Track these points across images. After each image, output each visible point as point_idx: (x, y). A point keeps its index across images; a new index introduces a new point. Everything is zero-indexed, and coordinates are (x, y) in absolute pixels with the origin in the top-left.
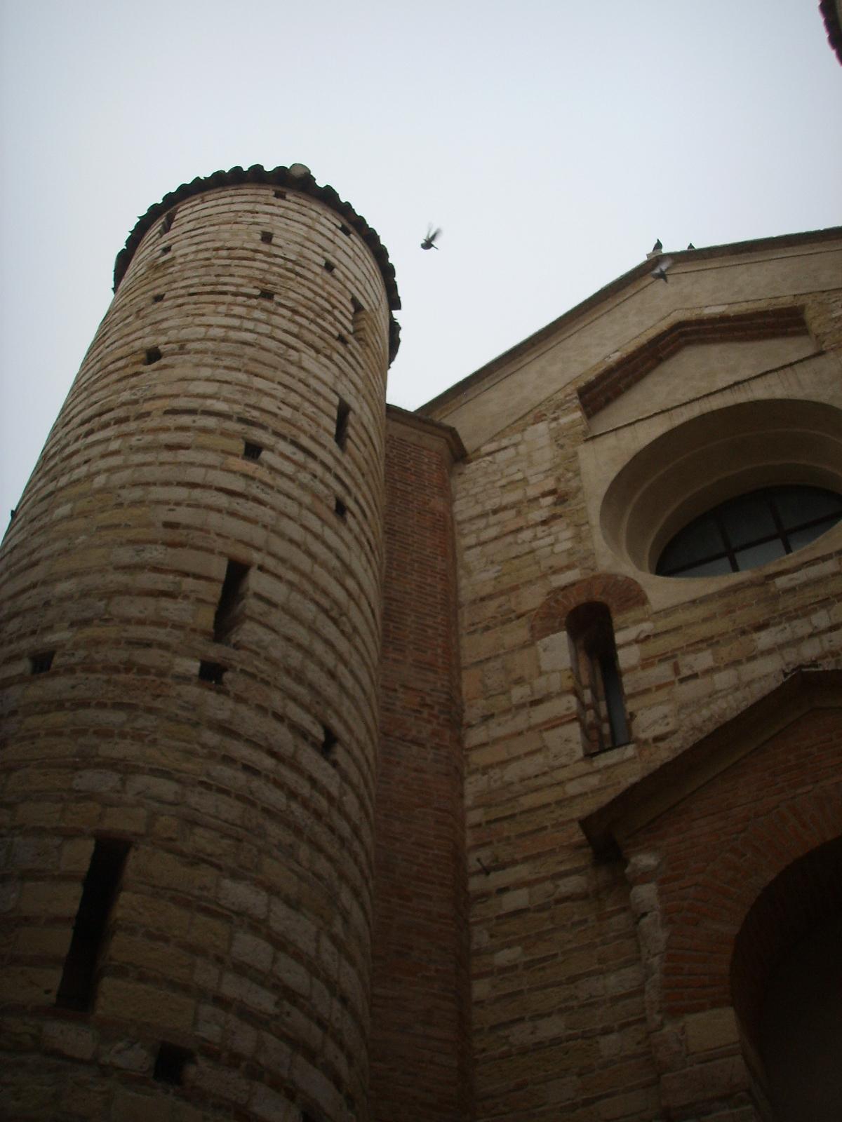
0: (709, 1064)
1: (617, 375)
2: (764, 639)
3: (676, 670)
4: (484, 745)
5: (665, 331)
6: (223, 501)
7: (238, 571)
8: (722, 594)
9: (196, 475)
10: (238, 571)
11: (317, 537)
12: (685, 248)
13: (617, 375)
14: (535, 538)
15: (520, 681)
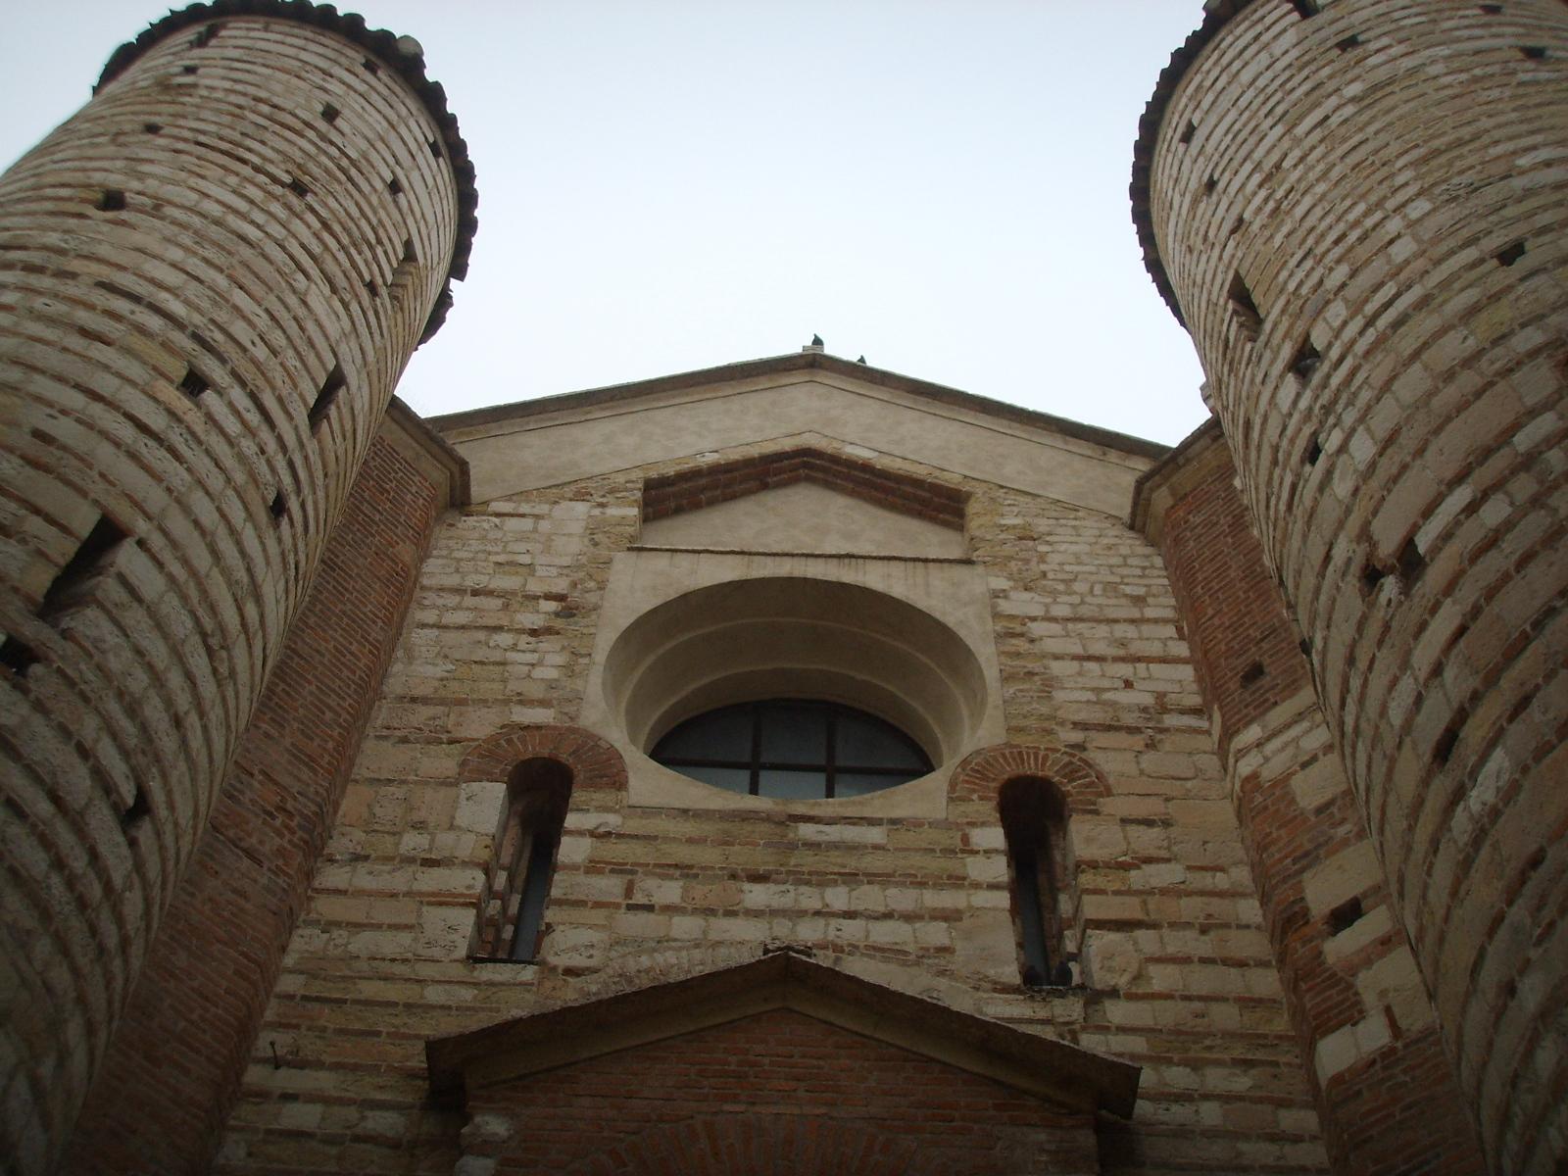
1: (703, 481)
2: (757, 895)
3: (629, 892)
4: (338, 892)
6: (127, 433)
7: (108, 534)
9: (106, 384)
10: (108, 534)
11: (232, 531)
12: (854, 358)
13: (703, 481)
14: (514, 648)
15: (419, 826)
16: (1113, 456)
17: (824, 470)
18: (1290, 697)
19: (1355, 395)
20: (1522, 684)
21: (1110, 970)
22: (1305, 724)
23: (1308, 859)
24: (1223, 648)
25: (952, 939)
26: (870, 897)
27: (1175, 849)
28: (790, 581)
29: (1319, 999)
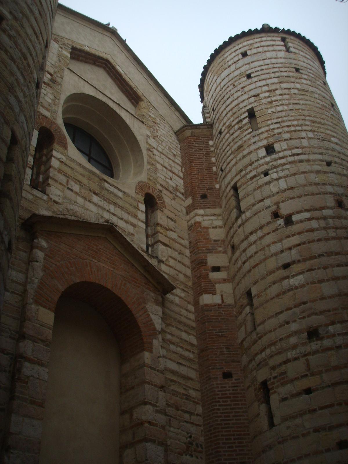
0: (42, 327)
1: (83, 54)
5: (103, 58)
8: (90, 171)
12: (124, 39)
13: (83, 54)
16: (173, 108)
17: (110, 69)
18: (213, 208)
19: (284, 170)
20: (312, 266)
21: (162, 255)
22: (216, 218)
23: (210, 251)
24: (197, 184)
25: (134, 232)
26: (119, 212)
27: (176, 229)
28: (105, 103)
29: (205, 285)
